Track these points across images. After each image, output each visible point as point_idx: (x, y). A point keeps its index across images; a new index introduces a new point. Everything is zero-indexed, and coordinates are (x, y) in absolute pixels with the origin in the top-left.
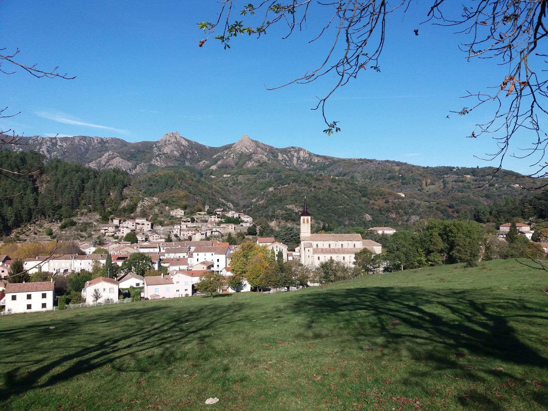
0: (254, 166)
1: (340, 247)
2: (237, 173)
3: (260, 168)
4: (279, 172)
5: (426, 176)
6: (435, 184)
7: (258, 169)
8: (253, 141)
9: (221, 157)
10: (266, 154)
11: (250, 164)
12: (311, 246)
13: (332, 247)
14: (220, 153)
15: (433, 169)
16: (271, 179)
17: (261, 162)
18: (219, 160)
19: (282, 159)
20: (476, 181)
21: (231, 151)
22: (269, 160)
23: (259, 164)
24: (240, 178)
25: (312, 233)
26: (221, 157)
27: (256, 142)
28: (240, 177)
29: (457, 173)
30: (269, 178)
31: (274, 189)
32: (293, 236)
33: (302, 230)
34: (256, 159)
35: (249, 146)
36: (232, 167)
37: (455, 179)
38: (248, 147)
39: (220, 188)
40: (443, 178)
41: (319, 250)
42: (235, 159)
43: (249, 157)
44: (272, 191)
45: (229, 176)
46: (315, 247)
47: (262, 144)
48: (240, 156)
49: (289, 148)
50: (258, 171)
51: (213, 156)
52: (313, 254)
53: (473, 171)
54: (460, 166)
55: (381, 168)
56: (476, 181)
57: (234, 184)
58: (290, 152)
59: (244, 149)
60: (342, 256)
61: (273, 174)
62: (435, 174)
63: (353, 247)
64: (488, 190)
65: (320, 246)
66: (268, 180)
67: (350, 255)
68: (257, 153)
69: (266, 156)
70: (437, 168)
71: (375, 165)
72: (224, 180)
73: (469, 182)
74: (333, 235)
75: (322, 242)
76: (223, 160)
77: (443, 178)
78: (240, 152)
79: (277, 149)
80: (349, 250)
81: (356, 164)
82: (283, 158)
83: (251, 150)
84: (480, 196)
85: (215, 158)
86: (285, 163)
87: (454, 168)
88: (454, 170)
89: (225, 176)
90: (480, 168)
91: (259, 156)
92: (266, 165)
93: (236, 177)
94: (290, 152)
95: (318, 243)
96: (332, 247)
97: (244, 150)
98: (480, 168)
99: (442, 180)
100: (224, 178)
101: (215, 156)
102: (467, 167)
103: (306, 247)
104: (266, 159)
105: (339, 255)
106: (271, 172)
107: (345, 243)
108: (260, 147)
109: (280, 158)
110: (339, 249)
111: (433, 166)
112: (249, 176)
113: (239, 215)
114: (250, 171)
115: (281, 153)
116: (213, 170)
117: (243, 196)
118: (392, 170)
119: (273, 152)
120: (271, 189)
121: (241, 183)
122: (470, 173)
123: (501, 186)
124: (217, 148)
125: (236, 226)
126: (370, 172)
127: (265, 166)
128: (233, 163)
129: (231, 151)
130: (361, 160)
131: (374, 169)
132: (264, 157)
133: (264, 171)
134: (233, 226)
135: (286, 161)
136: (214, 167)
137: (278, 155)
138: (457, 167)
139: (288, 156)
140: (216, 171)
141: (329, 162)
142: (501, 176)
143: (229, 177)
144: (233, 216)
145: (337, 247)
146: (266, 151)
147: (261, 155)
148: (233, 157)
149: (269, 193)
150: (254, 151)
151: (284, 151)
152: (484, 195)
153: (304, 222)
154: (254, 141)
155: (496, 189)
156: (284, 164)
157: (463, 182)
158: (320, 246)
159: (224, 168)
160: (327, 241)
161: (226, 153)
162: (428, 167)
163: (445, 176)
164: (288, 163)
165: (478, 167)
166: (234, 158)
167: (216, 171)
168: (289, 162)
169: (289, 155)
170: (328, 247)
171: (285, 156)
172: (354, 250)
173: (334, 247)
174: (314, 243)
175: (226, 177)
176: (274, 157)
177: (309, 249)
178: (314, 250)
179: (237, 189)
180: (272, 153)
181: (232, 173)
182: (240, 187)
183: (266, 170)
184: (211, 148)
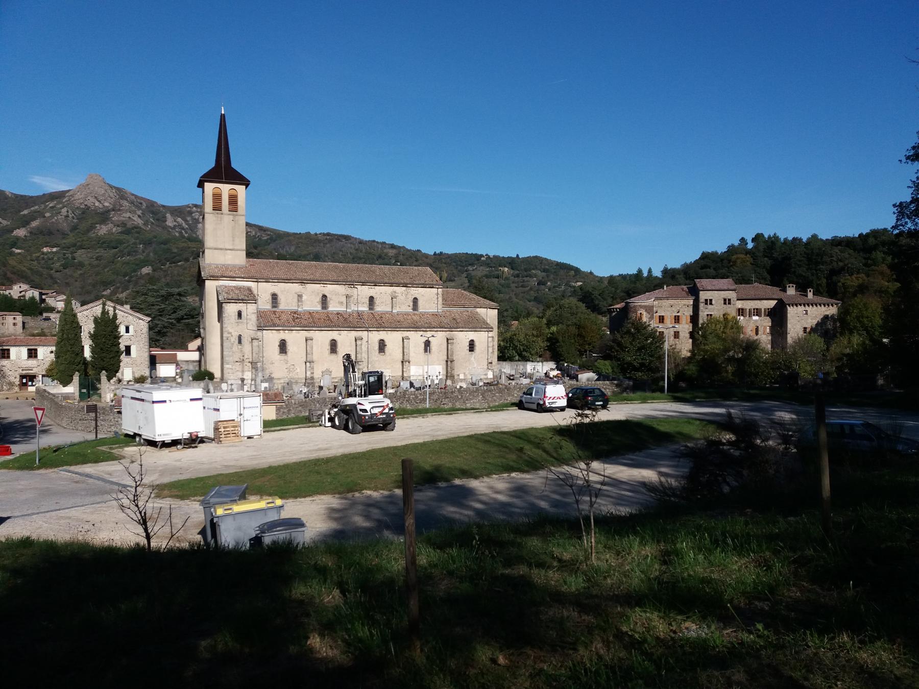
0: (112, 234)
1: (364, 308)
2: (74, 245)
3: (125, 236)
4: (165, 243)
5: (440, 268)
6: (454, 280)
7: (121, 238)
8: (111, 187)
9: (40, 214)
10: (139, 212)
11: (103, 230)
12: (249, 297)
13: (333, 307)
14: (37, 207)
15: (449, 256)
16: (148, 255)
17: (129, 225)
18: (34, 219)
19: (175, 226)
20: (518, 276)
21: (62, 203)
22: (145, 224)
23: (124, 229)
24: (81, 255)
25: (249, 255)
26: (40, 214)
27: (118, 189)
28: (80, 252)
29: (488, 264)
30: (145, 254)
31: (154, 270)
32: (182, 318)
33: (209, 241)
34: (119, 221)
35: (103, 195)
36: (63, 234)
37: (485, 273)
38: (101, 198)
39: (31, 269)
40: (466, 271)
41: (284, 317)
42: (70, 219)
43: (104, 216)
44: (148, 274)
45: (55, 250)
46: (265, 303)
47: (133, 195)
48: (83, 213)
49: (188, 206)
50: (120, 242)
51: (20, 211)
52: (260, 328)
53: (512, 262)
54: (491, 254)
55: (364, 251)
56: (518, 276)
57: (65, 267)
58: (190, 213)
59: (92, 200)
60: (375, 337)
61: (154, 245)
62: (454, 264)
63: (410, 310)
64: (538, 290)
65: (287, 303)
66: (142, 257)
67: (406, 334)
68: (119, 210)
69: (139, 216)
70: (456, 255)
71: (354, 244)
72: (43, 259)
73: (507, 279)
74: (337, 268)
75: (296, 287)
76: (42, 219)
77: (466, 271)
78: (83, 206)
79: (164, 206)
80: (400, 318)
81: (319, 241)
82: (175, 223)
83: (106, 204)
84: (527, 299)
85: (24, 215)
86: (180, 233)
87: (482, 256)
88: (482, 259)
89: (45, 250)
90: (520, 257)
91: (124, 215)
92: (138, 233)
93: (72, 253)
94: (190, 213)
95: (279, 288)
96: (333, 307)
97: (91, 201)
98: (520, 257)
99: (465, 275)
100: (43, 253)
101: (26, 212)
102: (501, 256)
103: (229, 301)
104: (140, 222)
105: (364, 334)
106: (148, 243)
107: (382, 293)
108: (127, 200)
109: (170, 222)
110: (360, 314)
111: (450, 252)
112: (101, 252)
113: (41, 294)
114: (104, 243)
115: (172, 214)
116: (18, 238)
117: (82, 288)
118: (383, 255)
119: (154, 211)
120: (146, 270)
121: (81, 265)
122: (507, 265)
123: (556, 285)
124: (32, 197)
125: (28, 319)
126: (345, 255)
127: (137, 235)
128: (65, 226)
129: (62, 203)
130: (328, 234)
131: (353, 251)
132: (135, 218)
133: (135, 243)
134: (20, 319)
135: (183, 229)
136: (21, 233)
137: (165, 217)
138: (487, 255)
139: (186, 221)
140: (24, 240)
141: (269, 235)
142: (553, 271)
143: (56, 253)
144: (24, 296)
145: (354, 308)
146: (139, 208)
147: (128, 215)
148: (65, 214)
149: (142, 277)
150: (114, 205)
151: (178, 211)
152: (533, 298)
153: (217, 207)
154: (115, 187)
155: (549, 290)
156: (177, 234)
157: (498, 277)
158: (287, 303)
159: (47, 234)
160: (314, 281)
161: (52, 207)
162: (441, 253)
163: (470, 268)
164: (186, 233)
165: (518, 255)
166: (67, 216)
167: (25, 239)
168: (189, 232)
169: (189, 219)
170: (319, 308)
171: (179, 220)
172: (415, 318)
173: (342, 309)
174: (264, 290)
175: (49, 253)
176: (158, 220)
177: (241, 306)
178: (261, 315)
179: (71, 276)
180: (153, 213)
181: (64, 245)
182: (79, 272)
183: (138, 241)
184: (17, 196)
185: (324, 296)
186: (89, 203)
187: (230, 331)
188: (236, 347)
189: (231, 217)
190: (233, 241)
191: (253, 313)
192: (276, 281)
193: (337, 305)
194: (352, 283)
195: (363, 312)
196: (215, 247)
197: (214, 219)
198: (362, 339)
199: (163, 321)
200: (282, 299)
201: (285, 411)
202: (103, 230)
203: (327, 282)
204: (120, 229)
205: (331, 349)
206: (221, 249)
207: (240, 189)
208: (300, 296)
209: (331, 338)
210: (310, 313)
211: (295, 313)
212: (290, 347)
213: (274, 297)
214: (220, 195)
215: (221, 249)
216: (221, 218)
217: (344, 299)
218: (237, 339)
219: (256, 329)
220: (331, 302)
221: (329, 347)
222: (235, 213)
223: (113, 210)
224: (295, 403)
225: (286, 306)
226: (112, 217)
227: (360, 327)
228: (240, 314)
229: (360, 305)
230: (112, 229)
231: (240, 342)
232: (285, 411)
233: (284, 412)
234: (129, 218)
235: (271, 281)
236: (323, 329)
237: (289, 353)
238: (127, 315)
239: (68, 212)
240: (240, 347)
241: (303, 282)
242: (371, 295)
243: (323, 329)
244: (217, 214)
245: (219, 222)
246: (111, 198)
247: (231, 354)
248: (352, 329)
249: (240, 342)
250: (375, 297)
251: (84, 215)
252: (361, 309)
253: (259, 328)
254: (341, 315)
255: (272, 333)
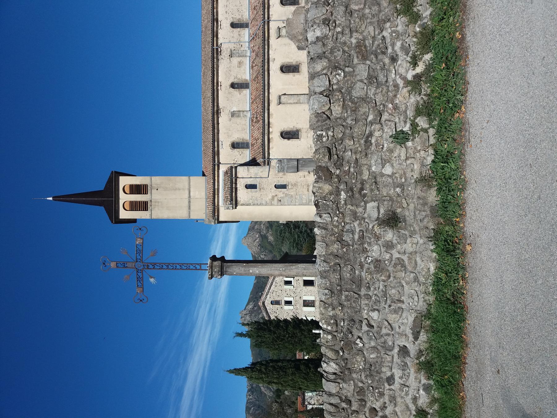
0: (272, 234)
1: (245, 34)
8: (248, 233)
11: (271, 238)
23: (270, 228)
27: (249, 230)
68: (260, 230)
75: (223, 119)
83: (257, 236)
91: (262, 227)
97: (256, 243)
108: (254, 226)
147: (262, 225)
150: (258, 232)
153: (143, 206)
170: (247, 92)
173: (247, 62)
185: (233, 86)
186: (257, 244)
187: (270, 197)
188: (290, 191)
189: (154, 191)
190: (179, 189)
191: (248, 170)
192: (216, 143)
193: (242, 69)
194: (215, 50)
195: (249, 34)
196: (187, 208)
197: (156, 209)
198: (279, 28)
199: (302, 226)
200: (236, 137)
201: (362, 71)
202: (271, 238)
203: (215, 81)
204: (270, 230)
205: (293, 72)
206: (190, 202)
207: (124, 181)
208: (233, 114)
209: (279, 72)
210: (252, 102)
211: (252, 121)
212: (288, 126)
213: (234, 146)
214: (131, 203)
215: (190, 202)
216: (156, 202)
217: (235, 60)
218: (280, 190)
219: (267, 167)
220: (239, 76)
221: (291, 75)
222: (149, 188)
223: (260, 233)
224: (326, 22)
225: (246, 132)
226: (264, 233)
227: (264, 33)
228: (249, 187)
229: (242, 39)
230: (270, 234)
231: (284, 187)
232: (362, 71)
233: (372, 79)
234: (264, 225)
235: (216, 149)
236: (266, 83)
237: (299, 126)
238: (274, 283)
239: (262, 255)
240: (290, 187)
241: (216, 112)
242: (229, 25)
243: (266, 83)
244: (151, 206)
245: (160, 204)
246: (254, 234)
247: (298, 197)
248: (266, 42)
249: (284, 187)
250: (232, 20)
251: (264, 247)
252: (247, 38)
253: (266, 163)
254: (253, 62)
255: (273, 148)
